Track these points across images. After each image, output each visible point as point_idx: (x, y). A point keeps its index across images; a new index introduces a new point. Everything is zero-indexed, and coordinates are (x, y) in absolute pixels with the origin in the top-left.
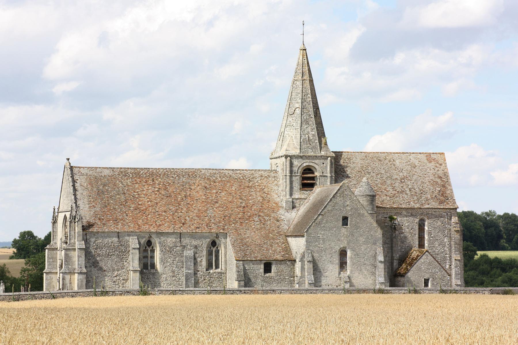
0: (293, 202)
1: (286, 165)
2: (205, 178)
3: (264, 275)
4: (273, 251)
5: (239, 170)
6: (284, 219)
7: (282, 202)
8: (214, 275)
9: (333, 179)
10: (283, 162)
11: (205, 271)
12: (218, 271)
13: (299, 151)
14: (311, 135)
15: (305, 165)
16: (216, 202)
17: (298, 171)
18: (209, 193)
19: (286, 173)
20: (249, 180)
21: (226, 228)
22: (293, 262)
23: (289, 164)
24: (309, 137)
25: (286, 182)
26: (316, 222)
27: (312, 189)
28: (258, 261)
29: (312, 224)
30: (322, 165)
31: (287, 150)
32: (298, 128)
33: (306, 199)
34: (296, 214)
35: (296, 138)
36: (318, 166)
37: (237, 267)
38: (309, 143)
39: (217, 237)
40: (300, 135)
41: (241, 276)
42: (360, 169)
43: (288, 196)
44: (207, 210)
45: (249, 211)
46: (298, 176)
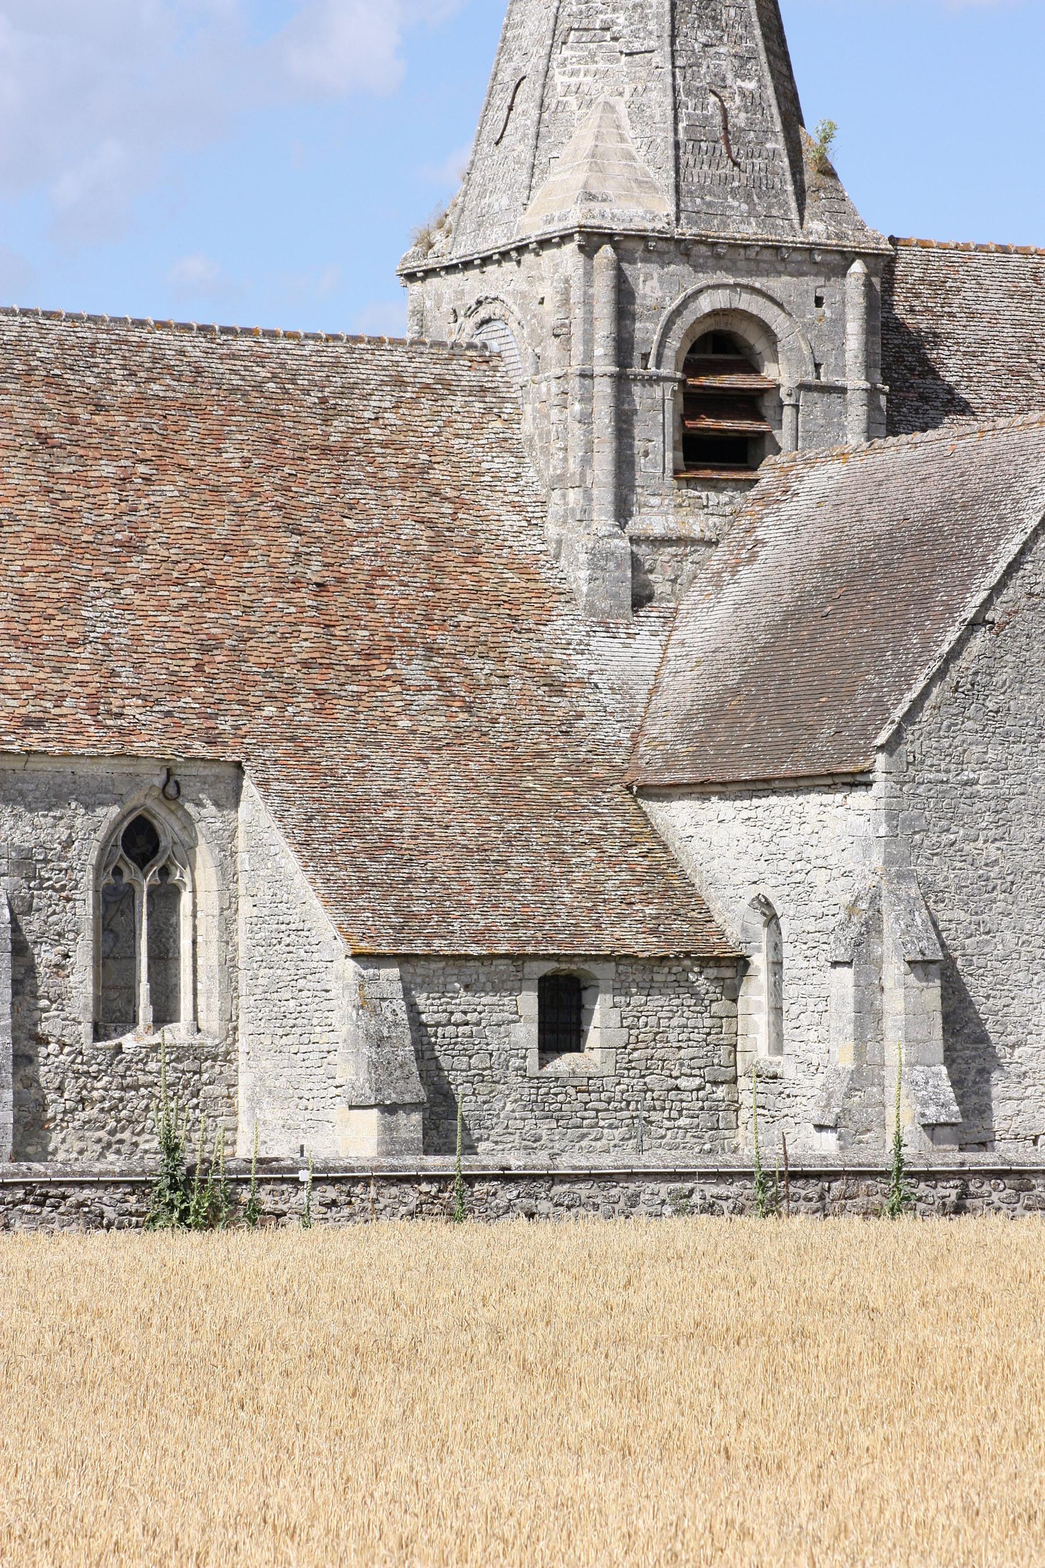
0: (636, 563)
1: (588, 302)
2: (30, 371)
3: (542, 1066)
4: (581, 891)
5: (247, 332)
6: (595, 678)
7: (557, 557)
8: (152, 1066)
9: (879, 408)
10: (567, 281)
11: (87, 1041)
12: (178, 1042)
13: (671, 209)
14: (737, 98)
15: (706, 304)
16: (131, 547)
17: (662, 344)
18: (71, 479)
19: (588, 356)
20: (323, 401)
21: (225, 724)
22: (728, 973)
23: (613, 296)
24: (725, 112)
25: (586, 419)
26: (953, 674)
27: (751, 476)
28: (502, 965)
29: (925, 693)
30: (812, 313)
31: (590, 197)
32: (653, 43)
33: (717, 543)
34: (665, 648)
35: (638, 111)
36: (790, 315)
37: (369, 1005)
38: (729, 151)
39: (171, 790)
40: (670, 92)
41: (398, 1073)
42: (1019, 356)
43: (603, 521)
44: (74, 597)
45: (358, 618)
46: (666, 379)
